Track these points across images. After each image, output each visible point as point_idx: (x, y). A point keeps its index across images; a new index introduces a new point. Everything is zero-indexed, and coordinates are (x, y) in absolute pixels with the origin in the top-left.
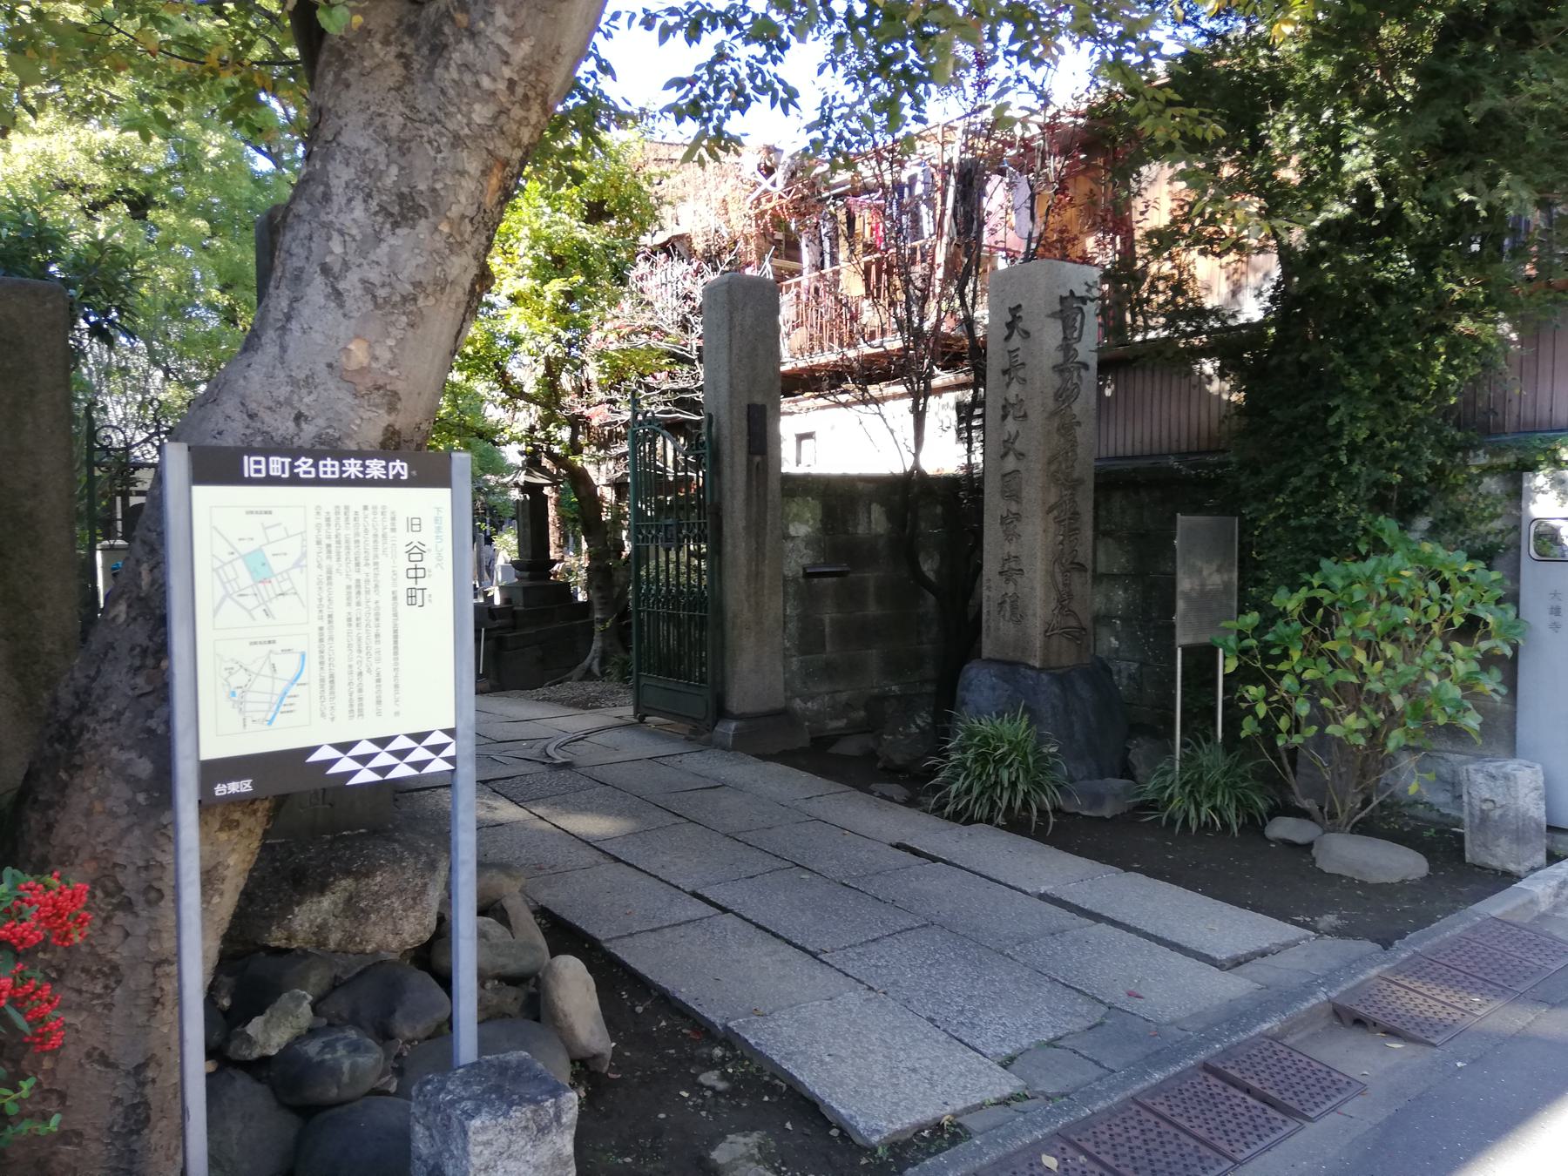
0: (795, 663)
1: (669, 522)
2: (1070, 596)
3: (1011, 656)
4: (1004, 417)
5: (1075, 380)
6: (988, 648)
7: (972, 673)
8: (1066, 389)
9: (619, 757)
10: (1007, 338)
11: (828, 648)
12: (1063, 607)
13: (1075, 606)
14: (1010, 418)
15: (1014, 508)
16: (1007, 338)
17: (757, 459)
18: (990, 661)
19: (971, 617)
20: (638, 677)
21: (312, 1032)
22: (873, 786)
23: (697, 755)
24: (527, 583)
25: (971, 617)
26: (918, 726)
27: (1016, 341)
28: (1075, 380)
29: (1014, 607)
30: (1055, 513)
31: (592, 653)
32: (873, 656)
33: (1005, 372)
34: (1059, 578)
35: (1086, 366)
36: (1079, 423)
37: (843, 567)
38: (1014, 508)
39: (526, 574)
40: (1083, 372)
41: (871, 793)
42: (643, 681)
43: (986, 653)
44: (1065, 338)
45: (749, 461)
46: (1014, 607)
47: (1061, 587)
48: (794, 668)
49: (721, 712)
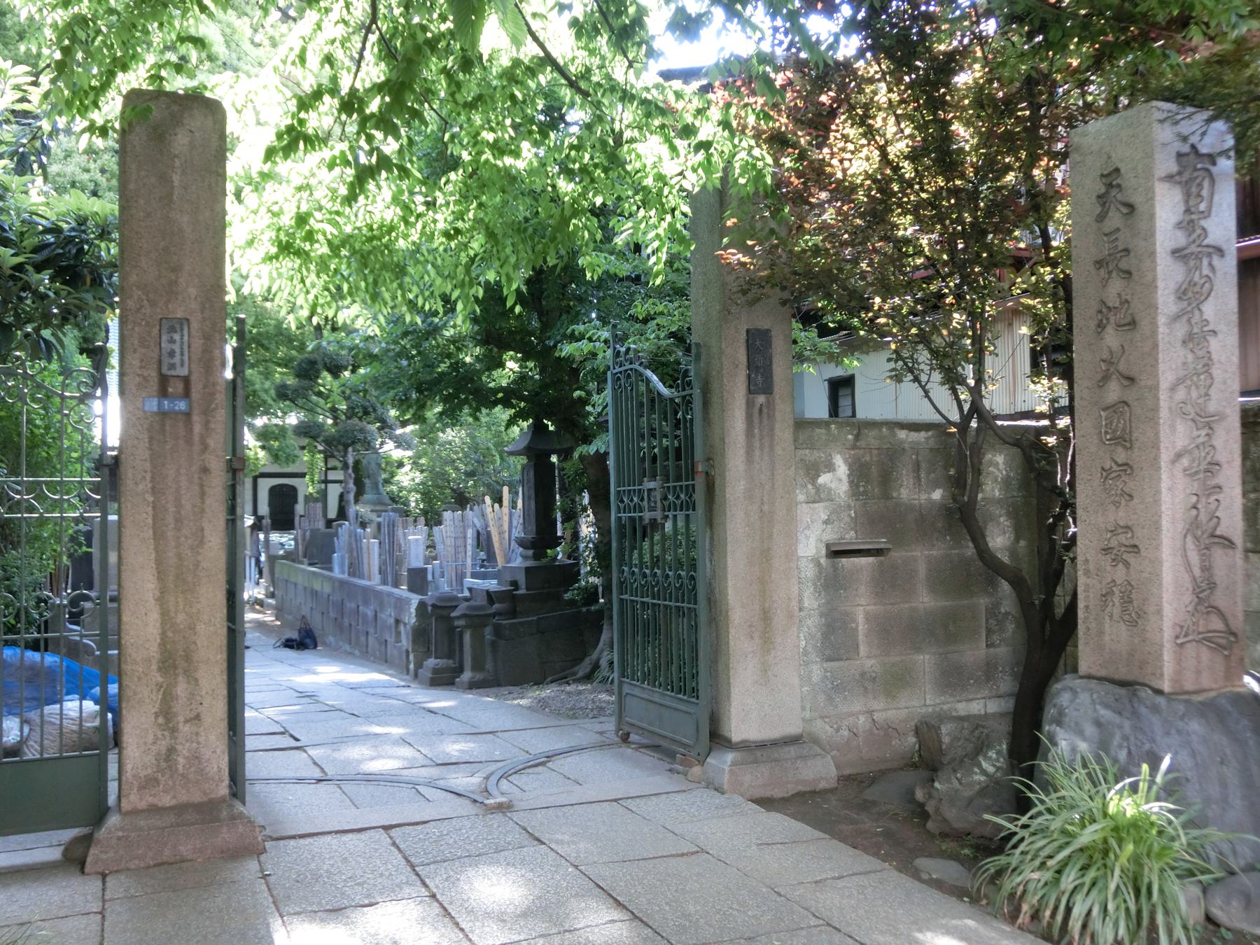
0: (817, 672)
1: (652, 485)
2: (1212, 586)
3: (1123, 674)
4: (1101, 326)
5: (1206, 271)
6: (1087, 657)
7: (1064, 699)
8: (1192, 284)
9: (578, 794)
10: (1101, 218)
11: (863, 649)
12: (1200, 601)
13: (1220, 600)
14: (1110, 330)
15: (1121, 456)
16: (1101, 218)
17: (761, 399)
18: (1089, 677)
19: (1059, 611)
20: (621, 683)
21: (1197, 516)
22: (922, 862)
23: (678, 798)
24: (530, 563)
25: (1059, 611)
26: (984, 772)
27: (1115, 219)
28: (1206, 271)
29: (1127, 601)
30: (1185, 462)
31: (601, 644)
32: (925, 661)
33: (1099, 264)
34: (1194, 558)
35: (1220, 251)
36: (1214, 333)
37: (882, 543)
38: (1121, 456)
39: (530, 552)
40: (1216, 261)
41: (916, 875)
42: (626, 689)
43: (1083, 668)
44: (1188, 211)
45: (750, 404)
46: (1127, 601)
47: (1197, 572)
48: (815, 679)
49: (717, 738)
